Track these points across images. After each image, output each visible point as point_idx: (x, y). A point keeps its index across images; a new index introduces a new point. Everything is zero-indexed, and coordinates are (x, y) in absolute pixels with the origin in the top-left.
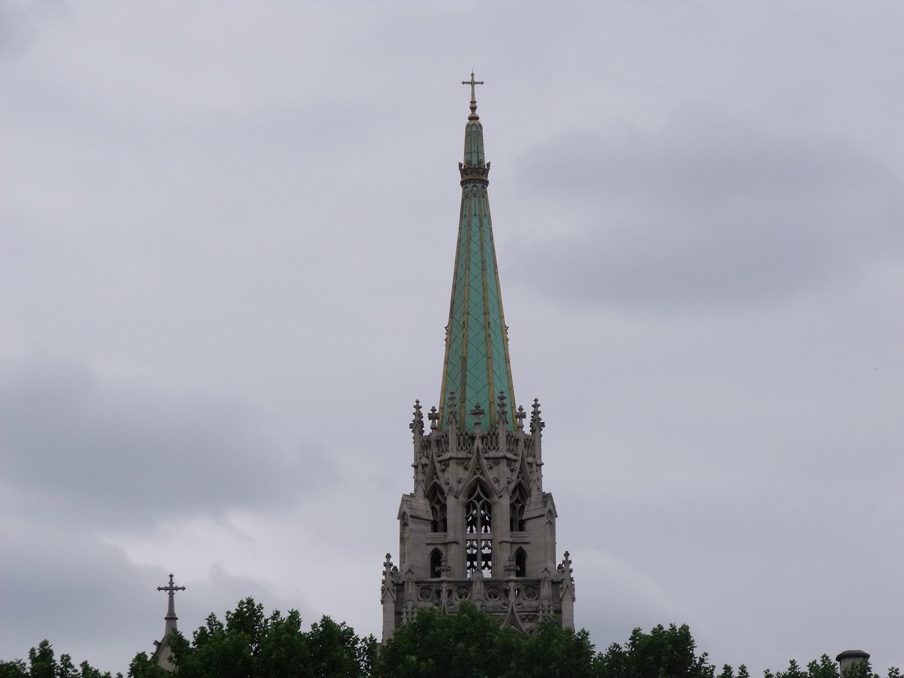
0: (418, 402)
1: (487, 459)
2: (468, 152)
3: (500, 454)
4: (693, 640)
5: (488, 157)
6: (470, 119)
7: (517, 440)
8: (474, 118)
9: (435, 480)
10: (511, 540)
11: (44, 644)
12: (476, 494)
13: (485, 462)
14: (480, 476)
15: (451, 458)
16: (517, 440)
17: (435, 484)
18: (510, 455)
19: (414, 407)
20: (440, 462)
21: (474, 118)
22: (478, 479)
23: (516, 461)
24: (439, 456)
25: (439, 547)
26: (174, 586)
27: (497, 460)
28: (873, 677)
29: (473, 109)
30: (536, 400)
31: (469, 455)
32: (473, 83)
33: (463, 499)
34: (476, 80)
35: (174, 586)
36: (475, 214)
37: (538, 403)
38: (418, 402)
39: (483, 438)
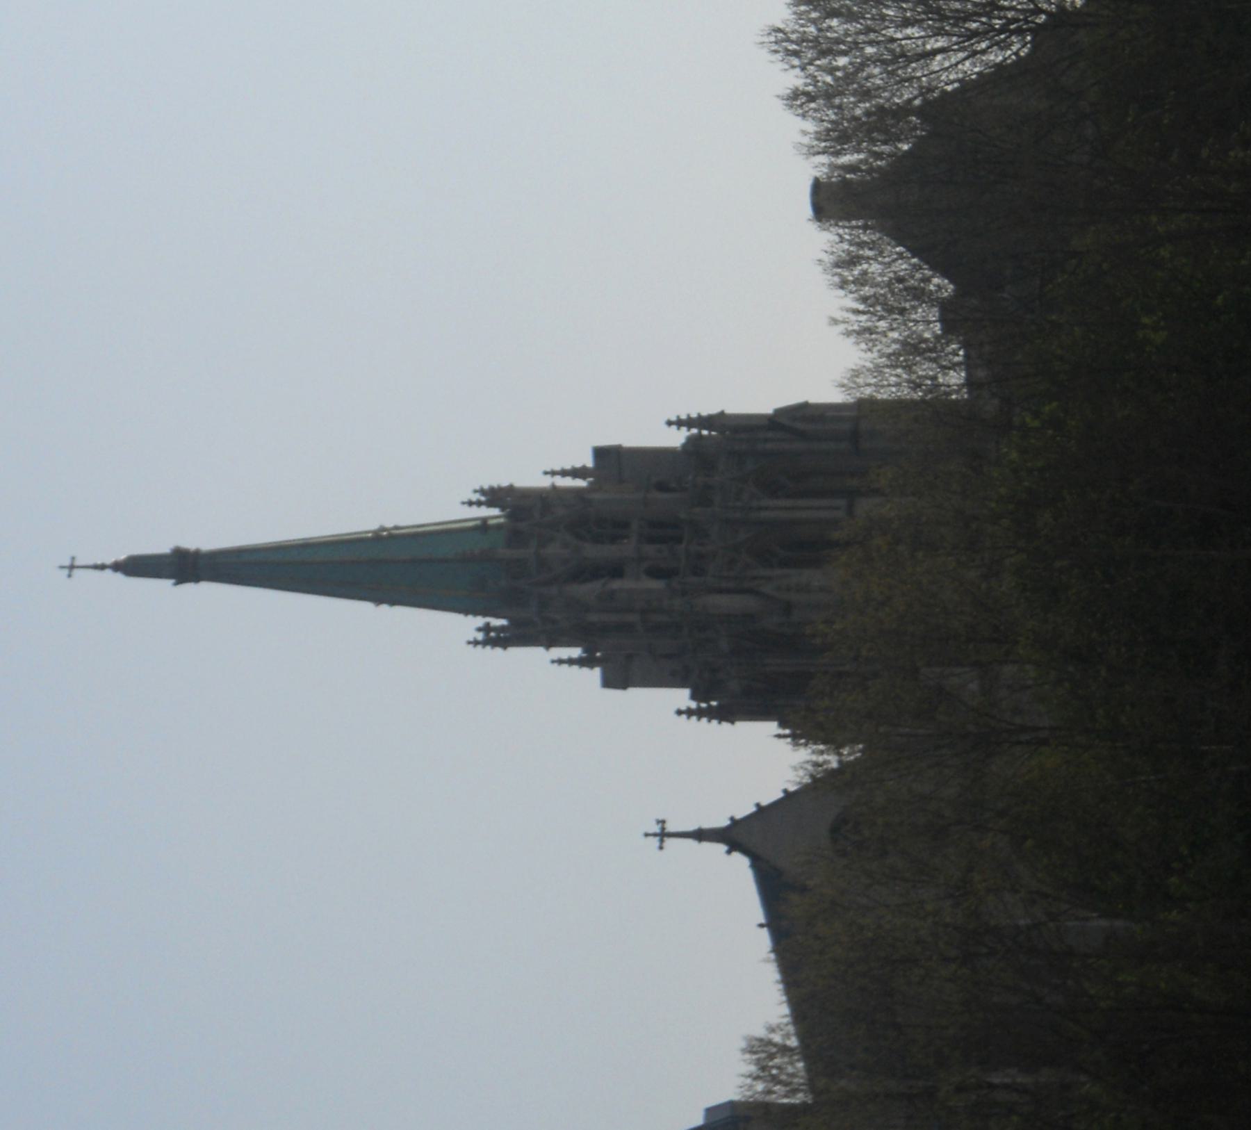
8: (117, 567)
21: (117, 567)
29: (102, 567)
32: (72, 567)
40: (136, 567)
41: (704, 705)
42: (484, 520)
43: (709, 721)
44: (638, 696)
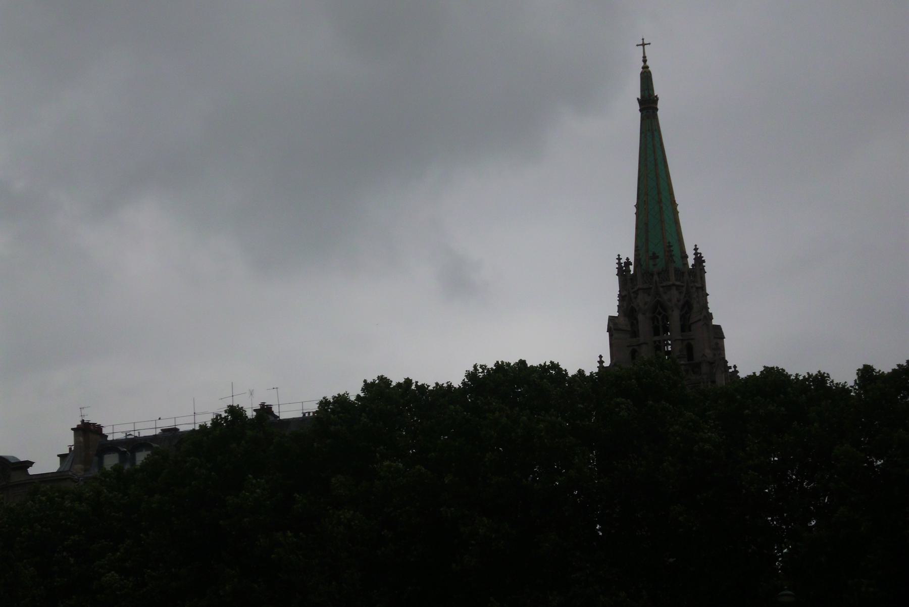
0: (619, 255)
2: (643, 90)
3: (671, 283)
5: (657, 92)
6: (643, 68)
7: (683, 273)
8: (645, 68)
9: (632, 305)
10: (681, 338)
11: (58, 456)
12: (658, 311)
13: (661, 289)
15: (639, 289)
16: (683, 273)
17: (632, 306)
18: (678, 283)
19: (617, 259)
20: (634, 292)
21: (645, 68)
23: (683, 286)
24: (632, 289)
27: (669, 287)
28: (230, 417)
29: (645, 61)
30: (696, 246)
31: (651, 286)
32: (643, 45)
34: (645, 42)
36: (649, 130)
37: (697, 247)
38: (619, 255)
39: (659, 274)
40: (646, 78)
41: (623, 265)
42: (686, 257)
43: (598, 367)
44: (604, 339)
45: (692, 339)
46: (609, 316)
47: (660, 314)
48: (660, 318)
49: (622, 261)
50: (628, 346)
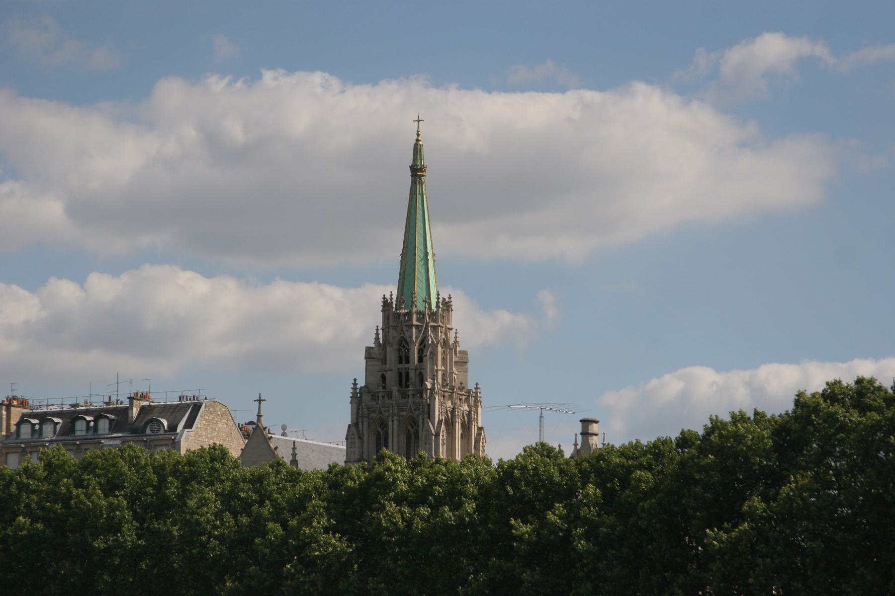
1: (406, 326)
4: (739, 412)
14: (403, 335)
22: (402, 337)
25: (384, 373)
26: (261, 399)
31: (398, 325)
32: (418, 121)
33: (395, 347)
34: (420, 119)
35: (261, 399)
41: (358, 391)
45: (423, 369)
46: (367, 347)
47: (404, 347)
48: (403, 349)
49: (358, 386)
50: (379, 371)
